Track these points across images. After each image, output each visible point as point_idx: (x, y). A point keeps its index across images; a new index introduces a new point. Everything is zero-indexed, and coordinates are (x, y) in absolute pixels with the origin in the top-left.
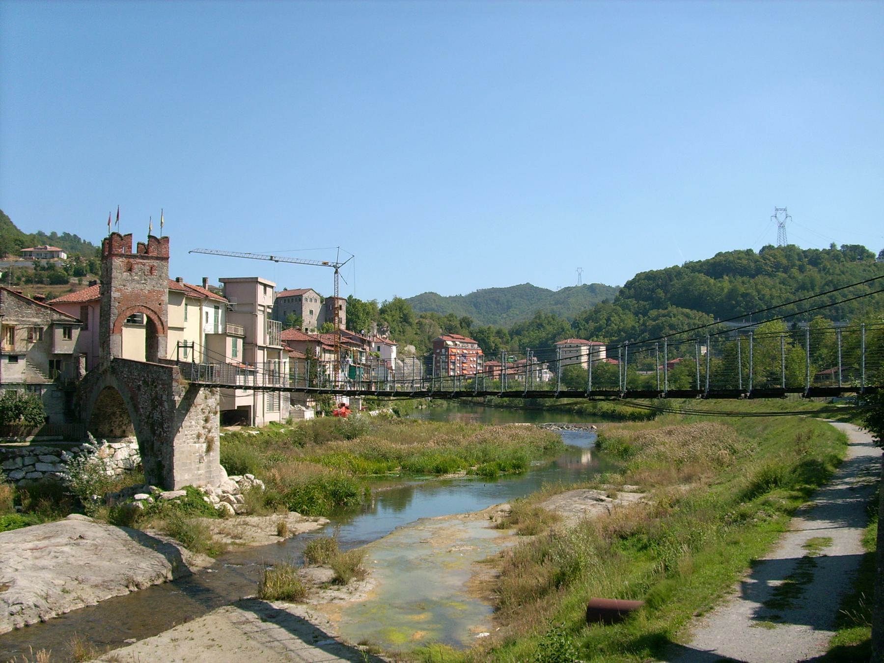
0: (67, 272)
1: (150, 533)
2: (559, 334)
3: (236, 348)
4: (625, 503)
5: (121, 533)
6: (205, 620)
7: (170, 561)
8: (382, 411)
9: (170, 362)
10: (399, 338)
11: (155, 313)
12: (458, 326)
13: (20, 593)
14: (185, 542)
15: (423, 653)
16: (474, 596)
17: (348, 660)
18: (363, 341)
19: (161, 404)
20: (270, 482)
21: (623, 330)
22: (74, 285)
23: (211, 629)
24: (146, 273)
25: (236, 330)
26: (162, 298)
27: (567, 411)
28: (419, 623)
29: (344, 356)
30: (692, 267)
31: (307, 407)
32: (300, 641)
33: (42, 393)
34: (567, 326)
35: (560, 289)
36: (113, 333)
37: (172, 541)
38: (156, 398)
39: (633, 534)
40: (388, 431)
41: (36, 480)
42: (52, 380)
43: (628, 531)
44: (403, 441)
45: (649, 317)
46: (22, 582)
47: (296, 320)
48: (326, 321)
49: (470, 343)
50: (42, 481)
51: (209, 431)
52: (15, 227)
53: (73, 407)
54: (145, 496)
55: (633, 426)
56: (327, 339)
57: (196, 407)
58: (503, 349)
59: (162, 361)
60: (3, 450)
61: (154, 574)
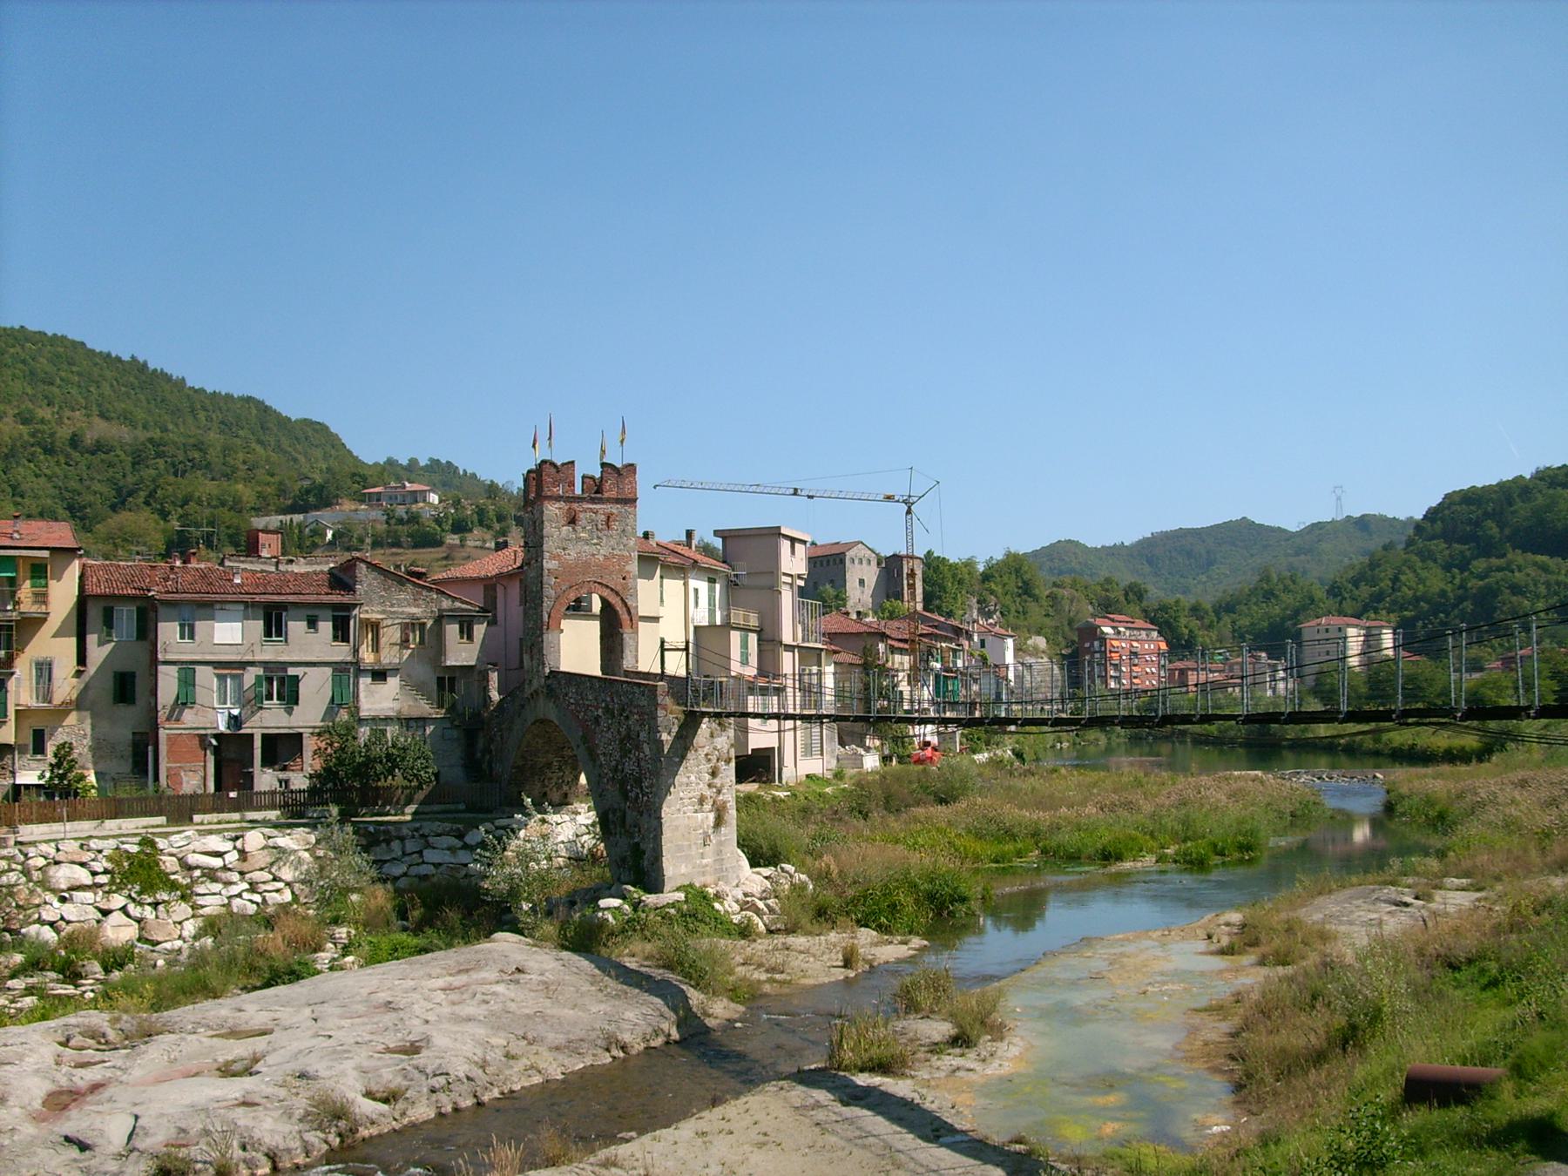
0: (440, 526)
1: (631, 964)
2: (1304, 608)
3: (747, 648)
4: (1451, 909)
5: (584, 963)
6: (746, 1103)
7: (674, 1009)
8: (995, 754)
9: (647, 675)
10: (1018, 624)
11: (617, 594)
12: (1122, 599)
13: (442, 1058)
14: (691, 979)
15: (1120, 1157)
16: (1195, 1065)
17: (998, 1165)
18: (958, 631)
19: (638, 748)
20: (822, 877)
21: (1423, 598)
22: (452, 547)
23: (760, 1116)
24: (600, 527)
25: (746, 618)
26: (627, 568)
27: (1328, 748)
28: (1105, 1108)
29: (925, 657)
30: (1549, 476)
31: (868, 749)
32: (911, 1136)
33: (428, 732)
34: (1320, 593)
35: (1302, 527)
36: (548, 629)
37: (670, 976)
38: (628, 737)
39: (1470, 961)
40: (1009, 788)
41: (425, 877)
42: (443, 711)
43: (1462, 956)
44: (1040, 805)
45: (1472, 573)
46: (440, 1040)
47: (837, 597)
48: (888, 597)
49: (1144, 629)
50: (435, 879)
51: (719, 792)
52: (350, 452)
53: (479, 755)
54: (616, 902)
55: (1452, 773)
56: (893, 628)
57: (696, 751)
58: (1203, 637)
59: (632, 675)
60: (371, 829)
61: (649, 1030)
